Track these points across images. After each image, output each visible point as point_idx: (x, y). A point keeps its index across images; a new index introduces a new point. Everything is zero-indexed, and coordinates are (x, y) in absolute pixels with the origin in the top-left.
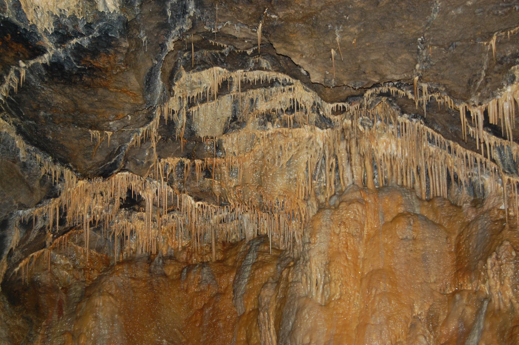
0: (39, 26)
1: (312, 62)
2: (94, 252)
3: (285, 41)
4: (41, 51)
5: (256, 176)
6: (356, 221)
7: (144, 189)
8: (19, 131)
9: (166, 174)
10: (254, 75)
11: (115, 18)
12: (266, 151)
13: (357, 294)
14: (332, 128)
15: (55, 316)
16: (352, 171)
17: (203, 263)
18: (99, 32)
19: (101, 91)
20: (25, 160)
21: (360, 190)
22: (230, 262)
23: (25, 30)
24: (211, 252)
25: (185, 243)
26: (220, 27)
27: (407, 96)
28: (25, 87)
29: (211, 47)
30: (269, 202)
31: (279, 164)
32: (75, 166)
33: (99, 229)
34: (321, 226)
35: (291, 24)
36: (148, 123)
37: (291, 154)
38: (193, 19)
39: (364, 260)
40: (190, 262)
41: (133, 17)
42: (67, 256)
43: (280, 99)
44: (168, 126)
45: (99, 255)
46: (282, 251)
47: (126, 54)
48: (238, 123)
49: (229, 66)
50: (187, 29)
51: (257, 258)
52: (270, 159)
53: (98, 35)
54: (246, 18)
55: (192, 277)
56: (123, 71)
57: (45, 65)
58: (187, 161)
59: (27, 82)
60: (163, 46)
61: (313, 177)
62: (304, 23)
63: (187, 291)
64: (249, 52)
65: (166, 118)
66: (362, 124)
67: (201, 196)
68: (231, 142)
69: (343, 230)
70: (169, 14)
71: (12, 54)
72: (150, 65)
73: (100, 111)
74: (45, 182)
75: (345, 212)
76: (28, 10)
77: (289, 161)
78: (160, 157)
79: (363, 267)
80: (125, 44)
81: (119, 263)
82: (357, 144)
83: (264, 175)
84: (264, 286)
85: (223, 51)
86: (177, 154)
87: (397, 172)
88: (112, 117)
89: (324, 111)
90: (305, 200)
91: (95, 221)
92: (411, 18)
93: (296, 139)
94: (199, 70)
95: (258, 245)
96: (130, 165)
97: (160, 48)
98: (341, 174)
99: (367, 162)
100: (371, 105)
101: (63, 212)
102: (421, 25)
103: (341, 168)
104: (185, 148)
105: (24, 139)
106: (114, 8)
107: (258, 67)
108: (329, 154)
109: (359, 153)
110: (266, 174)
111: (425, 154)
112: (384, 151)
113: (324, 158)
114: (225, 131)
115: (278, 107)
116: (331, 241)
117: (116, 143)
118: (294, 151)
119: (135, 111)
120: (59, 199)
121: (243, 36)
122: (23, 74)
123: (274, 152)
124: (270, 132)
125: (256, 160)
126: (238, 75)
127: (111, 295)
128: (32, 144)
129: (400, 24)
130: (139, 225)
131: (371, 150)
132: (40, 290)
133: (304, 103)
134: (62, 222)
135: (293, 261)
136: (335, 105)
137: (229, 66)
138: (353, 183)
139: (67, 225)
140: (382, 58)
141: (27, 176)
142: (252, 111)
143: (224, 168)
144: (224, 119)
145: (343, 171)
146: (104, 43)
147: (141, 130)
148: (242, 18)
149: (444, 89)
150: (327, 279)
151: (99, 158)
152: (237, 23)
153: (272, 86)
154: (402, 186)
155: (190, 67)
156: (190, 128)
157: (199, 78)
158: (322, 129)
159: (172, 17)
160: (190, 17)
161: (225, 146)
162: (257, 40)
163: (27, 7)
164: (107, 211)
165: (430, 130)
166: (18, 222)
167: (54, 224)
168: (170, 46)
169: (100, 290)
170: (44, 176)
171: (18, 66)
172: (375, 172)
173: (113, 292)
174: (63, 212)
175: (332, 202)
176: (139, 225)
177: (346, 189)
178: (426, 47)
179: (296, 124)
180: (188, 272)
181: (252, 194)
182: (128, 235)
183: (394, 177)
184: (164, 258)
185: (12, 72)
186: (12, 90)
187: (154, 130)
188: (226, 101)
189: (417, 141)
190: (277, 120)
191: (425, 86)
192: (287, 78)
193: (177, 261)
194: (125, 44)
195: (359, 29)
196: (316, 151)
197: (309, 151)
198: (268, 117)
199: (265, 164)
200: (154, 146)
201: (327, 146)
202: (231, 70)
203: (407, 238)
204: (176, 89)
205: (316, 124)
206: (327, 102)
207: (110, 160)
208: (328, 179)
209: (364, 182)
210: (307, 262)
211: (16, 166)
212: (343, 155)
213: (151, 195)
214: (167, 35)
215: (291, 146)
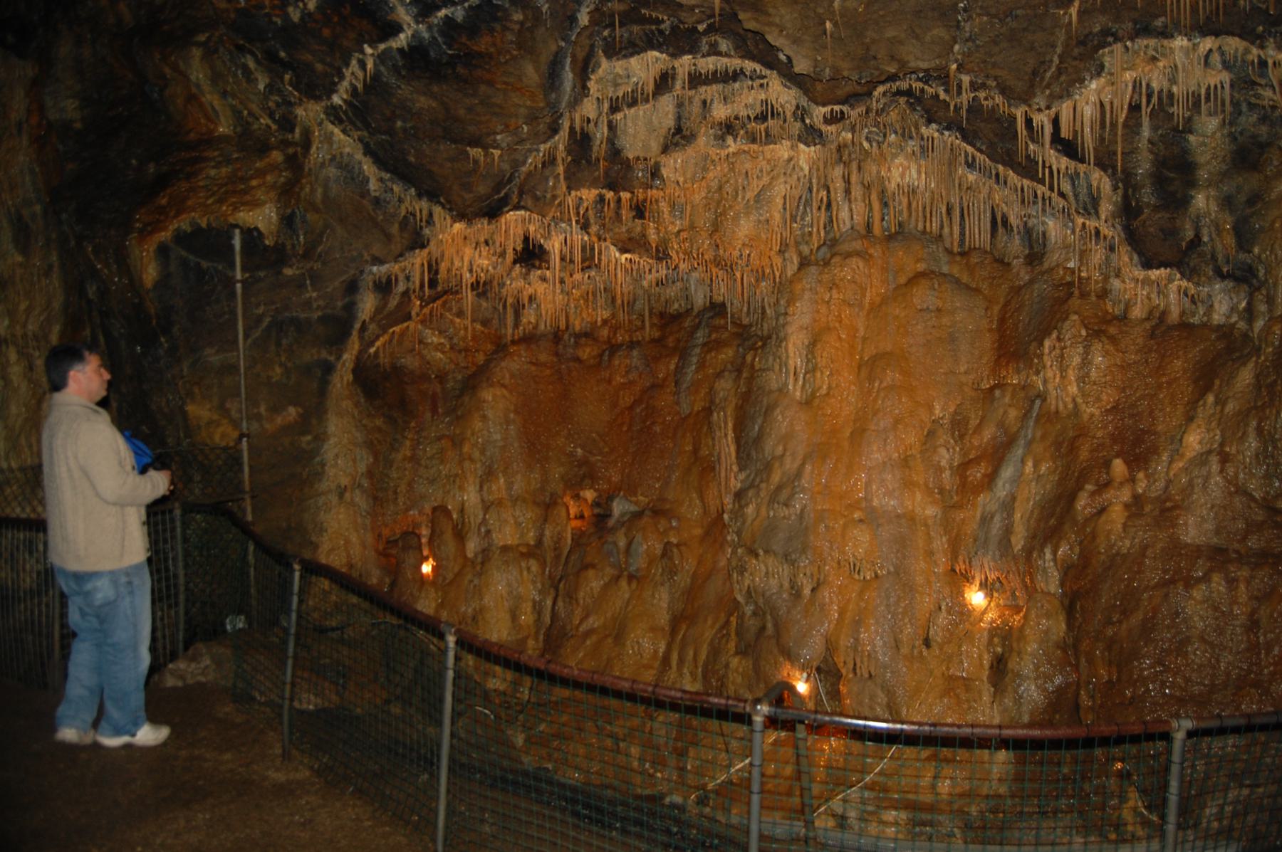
1: (796, 41)
4: (396, 29)
7: (548, 236)
8: (368, 151)
9: (578, 214)
10: (709, 64)
12: (724, 179)
14: (824, 145)
15: (428, 415)
16: (851, 210)
20: (377, 194)
27: (937, 96)
28: (375, 85)
31: (743, 198)
32: (449, 202)
34: (803, 290)
43: (746, 100)
48: (683, 137)
57: (400, 50)
58: (609, 195)
59: (376, 77)
60: (573, 19)
61: (793, 218)
63: (609, 382)
64: (701, 28)
66: (867, 139)
68: (673, 166)
69: (835, 295)
72: (554, 48)
77: (759, 195)
78: (569, 188)
80: (518, 16)
82: (859, 168)
85: (662, 27)
86: (594, 184)
87: (917, 211)
88: (500, 128)
89: (811, 118)
93: (769, 161)
94: (625, 57)
99: (874, 197)
100: (883, 110)
107: (714, 51)
110: (724, 214)
113: (810, 190)
114: (665, 150)
115: (743, 113)
116: (818, 312)
117: (506, 166)
118: (766, 180)
119: (532, 119)
122: (370, 65)
124: (731, 150)
126: (685, 63)
128: (387, 171)
130: (540, 288)
131: (881, 180)
132: (406, 379)
134: (433, 283)
136: (829, 108)
137: (671, 50)
139: (439, 289)
140: (903, 35)
141: (381, 217)
143: (662, 204)
144: (663, 132)
147: (542, 147)
149: (994, 84)
151: (482, 189)
153: (735, 81)
154: (924, 232)
155: (613, 51)
156: (613, 144)
157: (626, 69)
161: (664, 172)
162: (713, 9)
164: (494, 268)
165: (970, 149)
168: (584, 18)
170: (405, 217)
171: (362, 52)
178: (970, 17)
179: (769, 138)
183: (913, 219)
186: (354, 89)
187: (561, 147)
188: (667, 104)
189: (950, 164)
191: (966, 79)
192: (758, 67)
194: (518, 16)
198: (729, 128)
204: (592, 85)
205: (800, 139)
206: (817, 104)
207: (499, 192)
209: (869, 226)
212: (839, 184)
213: (557, 245)
215: (761, 171)
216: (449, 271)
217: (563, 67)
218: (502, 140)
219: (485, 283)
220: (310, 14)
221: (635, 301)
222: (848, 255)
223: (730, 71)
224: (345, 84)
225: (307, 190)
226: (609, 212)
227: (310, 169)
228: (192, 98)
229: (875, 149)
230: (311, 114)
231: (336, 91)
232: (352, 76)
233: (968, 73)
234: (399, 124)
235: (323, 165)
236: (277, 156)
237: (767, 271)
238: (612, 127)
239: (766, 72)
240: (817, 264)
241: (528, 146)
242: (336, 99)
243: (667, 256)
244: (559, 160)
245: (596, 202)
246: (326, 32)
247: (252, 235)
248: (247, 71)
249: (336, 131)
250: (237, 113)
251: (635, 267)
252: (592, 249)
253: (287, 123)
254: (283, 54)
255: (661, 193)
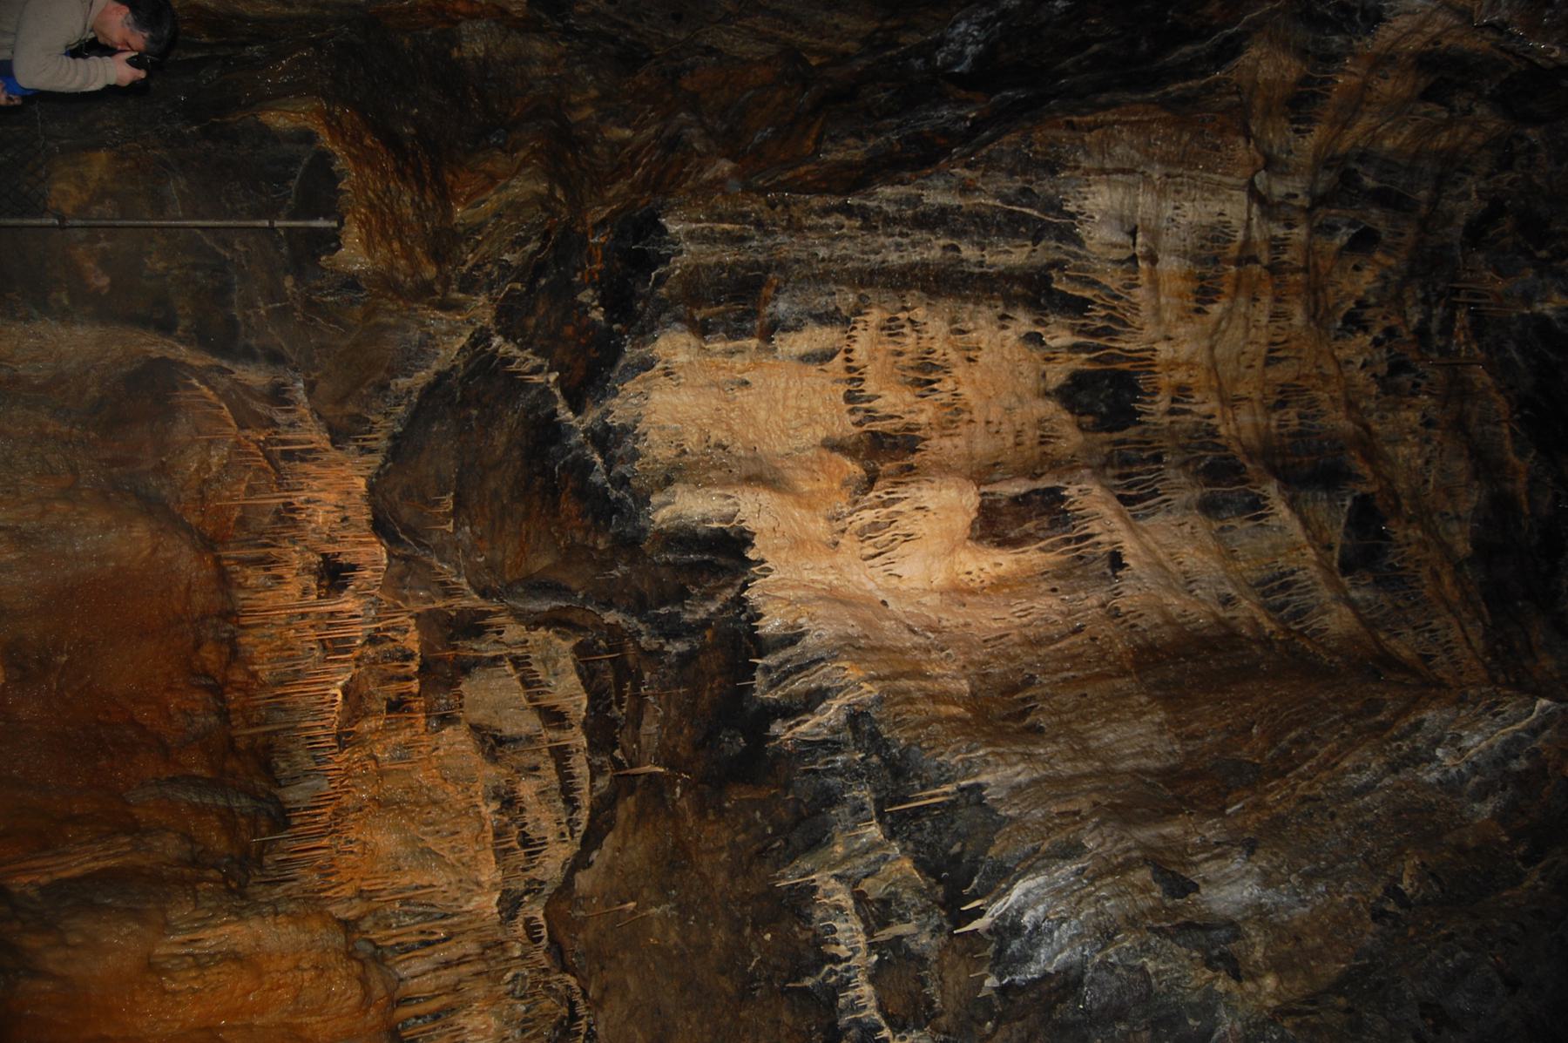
0: (617, 401)
1: (610, 869)
2: (236, 514)
3: (640, 817)
4: (577, 408)
7: (358, 594)
8: (441, 376)
9: (387, 630)
10: (580, 766)
12: (447, 806)
13: (177, 1025)
14: (500, 923)
16: (424, 973)
17: (228, 712)
18: (617, 498)
19: (521, 508)
21: (390, 995)
22: (232, 764)
23: (609, 379)
24: (250, 725)
25: (265, 676)
26: (651, 699)
28: (516, 384)
29: (619, 685)
30: (351, 824)
31: (425, 833)
33: (282, 519)
34: (311, 932)
35: (670, 824)
36: (477, 591)
37: (445, 853)
38: (660, 651)
39: (249, 1027)
40: (228, 689)
42: (225, 466)
43: (543, 819)
44: (472, 625)
45: (231, 524)
46: (261, 861)
47: (586, 547)
48: (492, 748)
50: (642, 644)
51: (242, 815)
52: (433, 815)
54: (670, 743)
55: (197, 697)
56: (556, 542)
57: (554, 413)
58: (414, 666)
59: (525, 386)
60: (609, 605)
61: (406, 901)
62: (675, 846)
63: (169, 689)
64: (617, 753)
65: (488, 621)
66: (516, 976)
67: (352, 698)
68: (455, 740)
69: (307, 976)
71: (567, 359)
72: (574, 586)
73: (487, 510)
74: (358, 422)
77: (431, 852)
78: (418, 616)
79: (235, 1027)
80: (602, 544)
81: (218, 560)
82: (478, 974)
83: (401, 808)
84: (187, 837)
85: (615, 708)
86: (426, 646)
88: (478, 530)
89: (529, 903)
90: (360, 893)
91: (294, 511)
93: (474, 858)
94: (578, 669)
95: (269, 814)
96: (399, 567)
97: (604, 600)
98: (419, 953)
100: (550, 989)
101: (307, 455)
103: (428, 950)
104: (439, 660)
106: (658, 520)
107: (596, 772)
109: (460, 981)
110: (403, 811)
112: (470, 1027)
113: (445, 917)
114: (475, 728)
115: (528, 818)
117: (436, 539)
118: (451, 858)
119: (491, 566)
120: (329, 446)
121: (643, 740)
122: (536, 379)
124: (483, 809)
127: (155, 550)
128: (421, 398)
129: (693, 1020)
134: (289, 456)
135: (240, 885)
136: (543, 923)
137: (591, 721)
138: (401, 980)
139: (282, 463)
140: (631, 997)
142: (518, 772)
143: (408, 733)
144: (496, 724)
146: (601, 508)
147: (463, 580)
148: (669, 736)
150: (203, 960)
151: (406, 512)
152: (661, 728)
156: (475, 665)
158: (498, 904)
159: (658, 615)
160: (662, 646)
161: (448, 731)
162: (638, 765)
163: (645, 380)
164: (314, 530)
167: (284, 442)
168: (611, 617)
169: (162, 530)
170: (368, 420)
171: (551, 370)
173: (161, 554)
174: (307, 455)
175: (362, 945)
176: (293, 588)
179: (502, 854)
180: (207, 688)
181: (363, 791)
182: (274, 572)
184: (232, 642)
185: (539, 361)
186: (510, 361)
187: (466, 603)
188: (529, 723)
192: (582, 827)
193: (228, 664)
194: (602, 544)
195: (676, 945)
196: (456, 899)
198: (509, 802)
201: (468, 917)
202: (584, 725)
204: (542, 632)
205: (505, 892)
207: (403, 532)
209: (406, 1001)
210: (237, 914)
211: (382, 373)
212: (455, 951)
213: (348, 606)
214: (628, 611)
215: (461, 851)
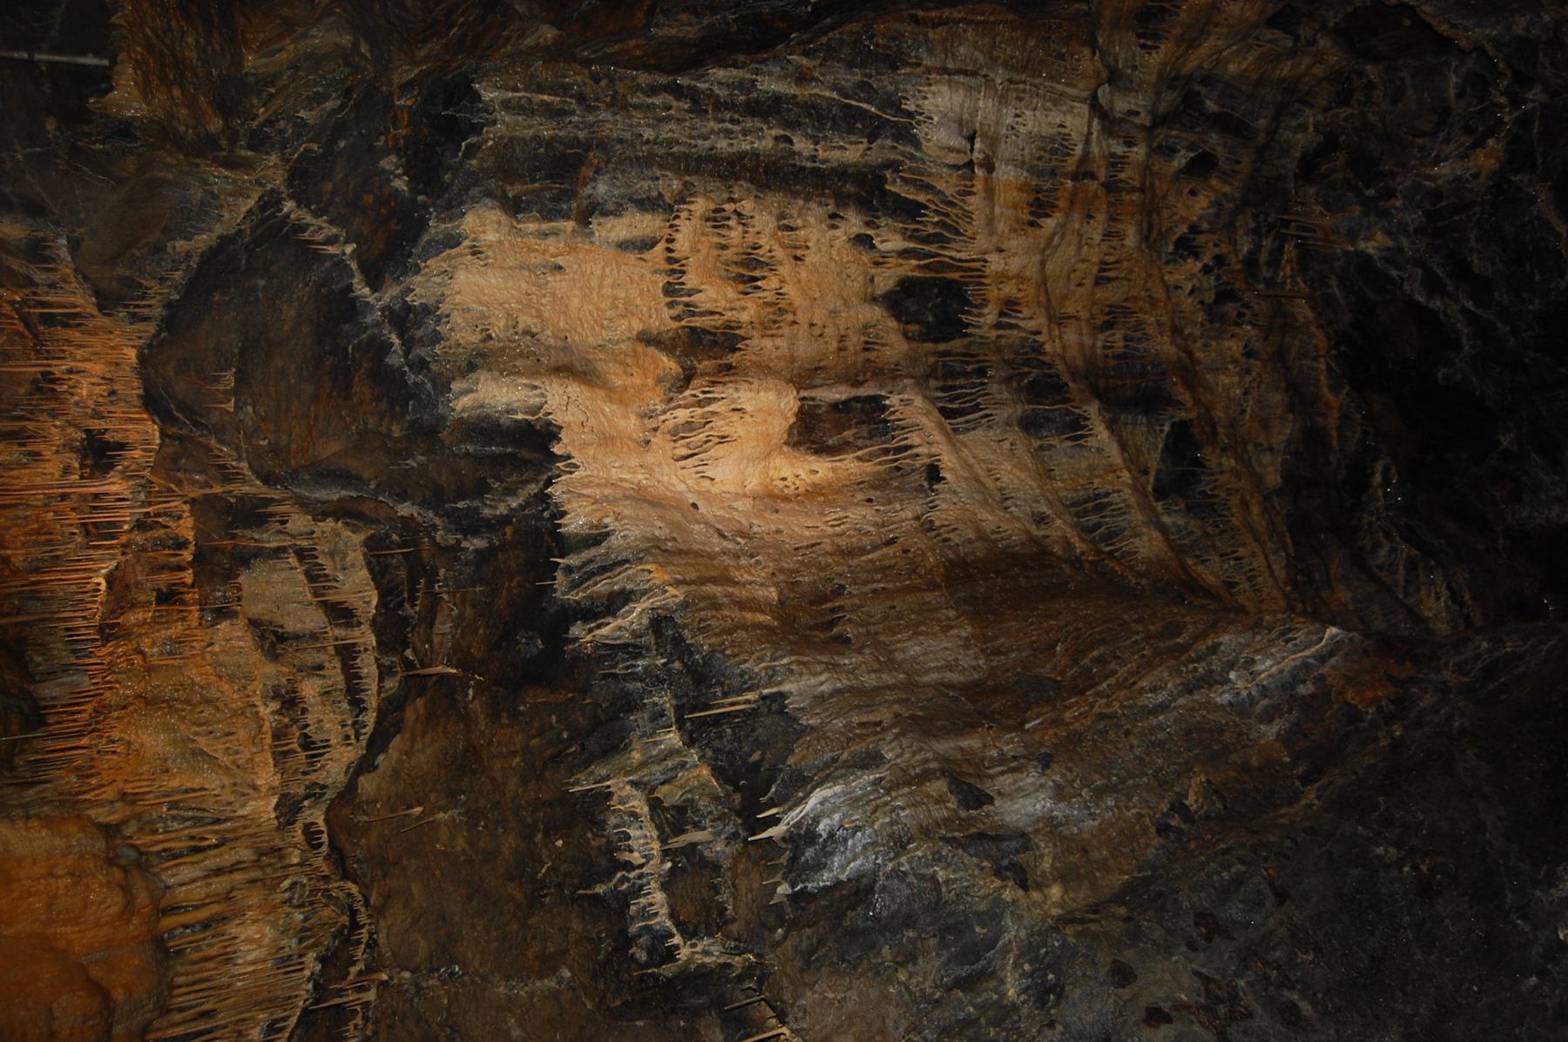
0: (419, 278)
1: (396, 774)
4: (375, 285)
5: (168, 691)
6: (85, 906)
7: (126, 476)
8: (224, 241)
9: (158, 515)
10: (368, 666)
11: (441, 410)
12: (221, 705)
14: (278, 829)
16: (193, 881)
20: (169, 250)
23: (410, 255)
26: (445, 596)
27: (354, 963)
28: (308, 254)
29: (412, 582)
30: (114, 723)
31: (196, 734)
32: (161, 344)
33: (40, 390)
34: (67, 836)
38: (457, 548)
41: (447, 442)
43: (327, 721)
44: (254, 514)
48: (273, 645)
49: (380, 619)
50: (438, 539)
53: (410, 382)
54: (464, 644)
57: (349, 288)
58: (187, 555)
59: (319, 257)
60: (403, 497)
61: (174, 805)
64: (409, 653)
65: (271, 509)
66: (294, 884)
68: (232, 636)
69: (62, 883)
70: (460, 505)
72: (366, 475)
75: (104, 880)
76: (444, 260)
77: (202, 753)
78: (193, 502)
80: (397, 431)
82: (253, 881)
85: (407, 606)
86: (201, 535)
87: (202, 970)
88: (262, 411)
89: (310, 807)
90: (123, 796)
92: (494, 945)
93: (250, 760)
94: (369, 563)
99: (215, 908)
100: (330, 897)
101: (70, 320)
102: (690, 933)
105: (211, 248)
106: (459, 408)
107: (385, 672)
108: (226, 831)
109: (233, 889)
110: (172, 710)
111: (243, 1020)
112: (243, 937)
113: (217, 821)
114: (254, 624)
115: (310, 718)
116: (34, 863)
117: (215, 418)
118: (225, 760)
119: (275, 450)
120: (95, 312)
121: (436, 640)
122: (331, 250)
123: (220, 722)
124: (261, 709)
125: (201, 687)
126: (366, 637)
128: (200, 265)
129: (480, 928)
130: (52, 467)
131: (241, 913)
133: (323, 766)
134: (49, 320)
136: (324, 828)
137: (380, 619)
138: (168, 887)
139: (41, 328)
140: (415, 905)
141: (138, 253)
143: (180, 626)
144: (278, 620)
145: (192, 863)
147: (245, 465)
149: (369, 1033)
151: (181, 387)
152: (455, 627)
153: (350, 703)
154: (172, 987)
155: (374, 547)
156: (256, 557)
157: (353, 566)
160: (459, 542)
161: (224, 626)
162: (430, 666)
163: (450, 257)
164: (77, 404)
165: (294, 1020)
166: (41, 234)
168: (405, 510)
170: (141, 285)
171: (347, 242)
172: (198, 927)
174: (70, 320)
175: (126, 851)
177: (155, 875)
178: (444, 982)
179: (281, 757)
181: (128, 687)
182: (29, 448)
183: (189, 968)
186: (303, 229)
187: (246, 489)
188: (314, 620)
189: (270, 1000)
190: (286, 720)
191: (371, 995)
192: (369, 730)
194: (397, 431)
195: (463, 851)
197: (227, 791)
198: (290, 702)
199: (194, 706)
200: (213, 491)
201: (242, 822)
203: (54, 1019)
204: (329, 524)
205: (284, 796)
206: (328, 810)
207: (178, 409)
208: (173, 835)
209: (174, 909)
212: (227, 858)
213: (114, 488)
214: (424, 504)
215: (237, 753)
216: (69, 342)
217: (343, 488)
218: (246, 414)
219: (53, 390)
220: (389, 181)
221: (39, 600)
222: (126, 890)
223: (362, 696)
224: (309, 218)
225: (169, 160)
226: (163, 556)
227: (197, 166)
228: (289, 27)
229: (280, 897)
230: (270, 172)
231: (299, 206)
232: (319, 228)
233: (379, 996)
234: (262, 283)
235: (205, 182)
236: (215, 125)
237: (94, 781)
238: (278, 552)
239: (364, 740)
240: (108, 848)
241: (244, 447)
242: (289, 205)
243: (106, 639)
244: (230, 487)
245: (176, 538)
246: (369, 199)
247: (102, 81)
248: (321, 98)
249: (251, 202)
250: (272, 80)
251: (87, 597)
252: (113, 536)
253: (259, 142)
254: (342, 144)
255: (195, 624)
